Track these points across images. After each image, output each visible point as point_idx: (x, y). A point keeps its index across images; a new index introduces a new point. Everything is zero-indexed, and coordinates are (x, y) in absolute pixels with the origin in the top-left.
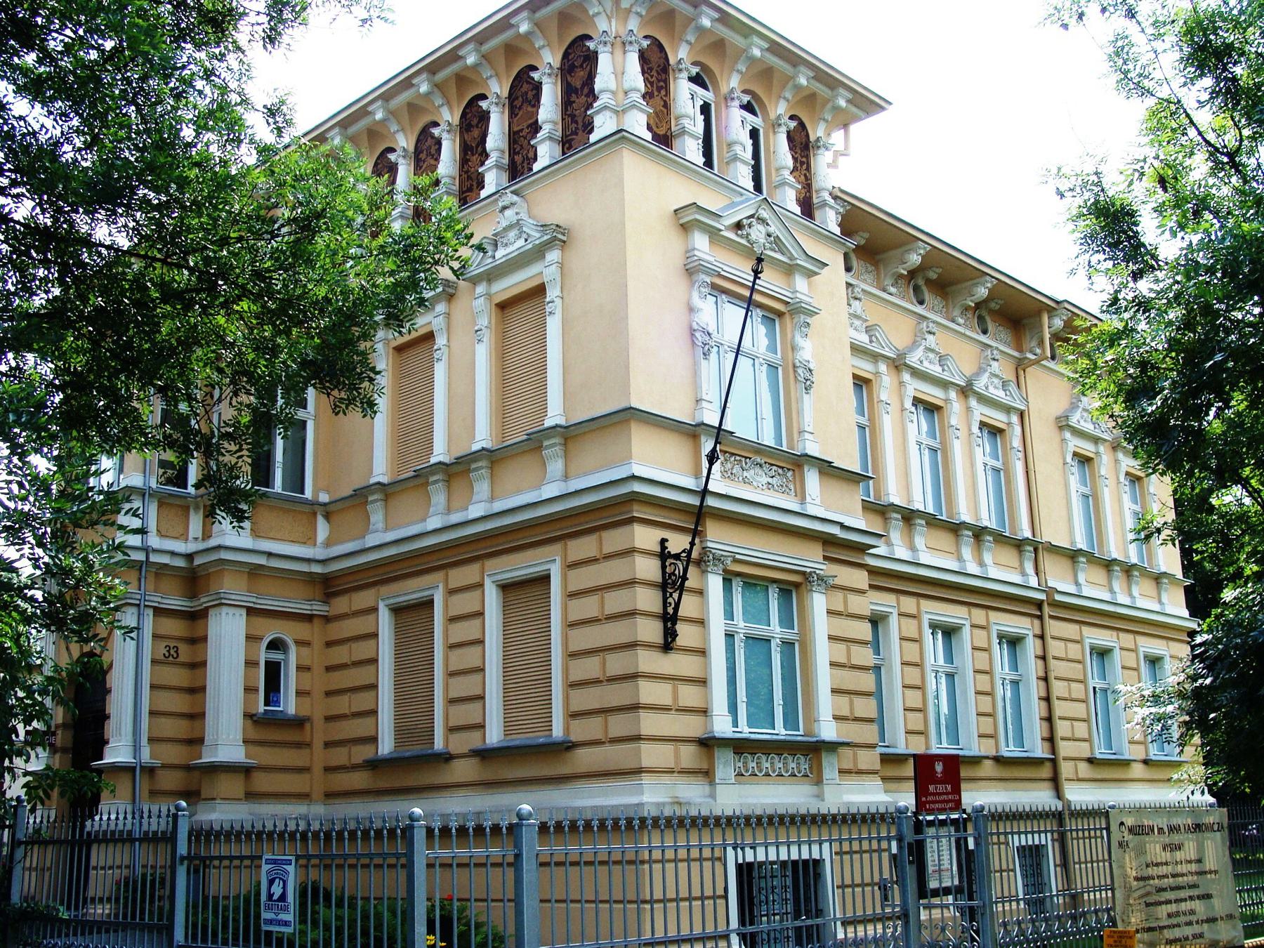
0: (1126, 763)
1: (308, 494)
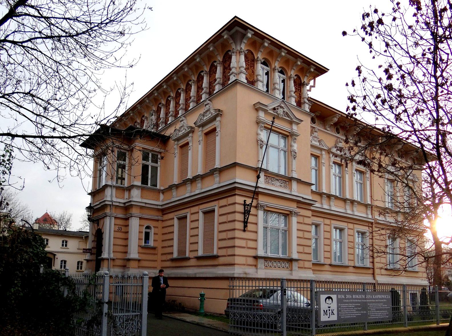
0: (323, 265)
1: (158, 187)
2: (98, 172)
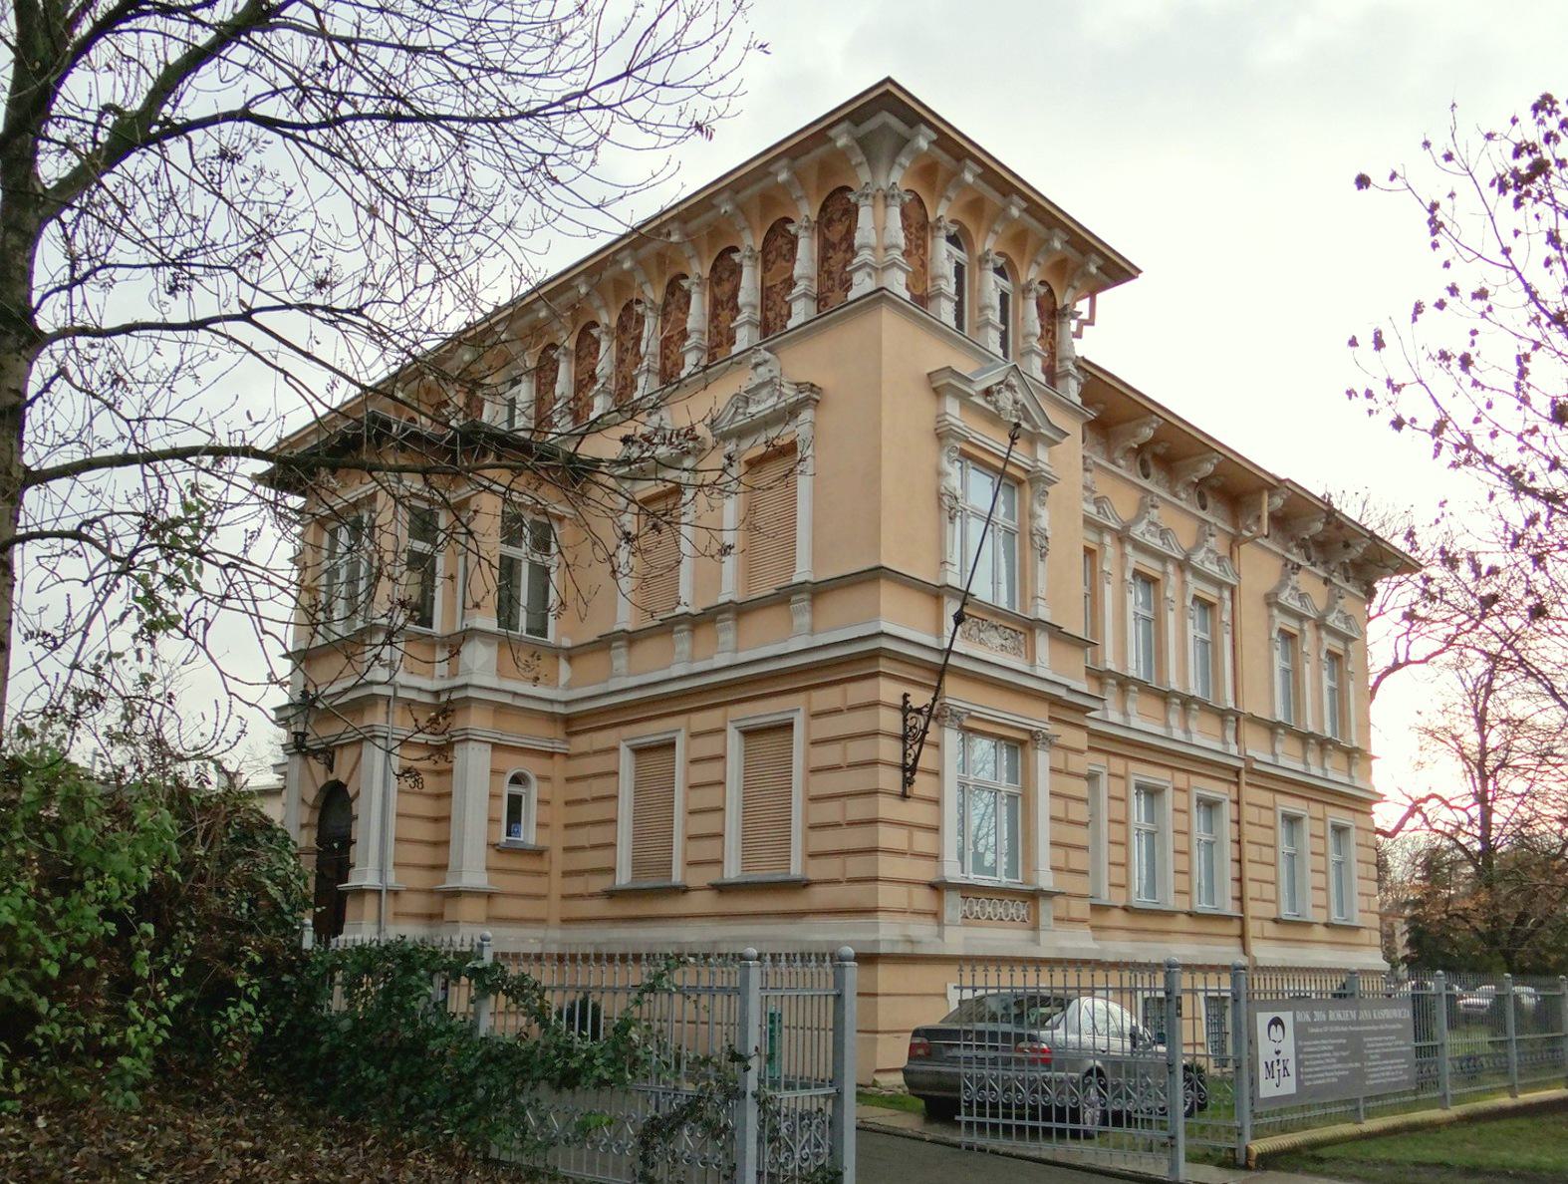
0: (1309, 925)
1: (551, 638)
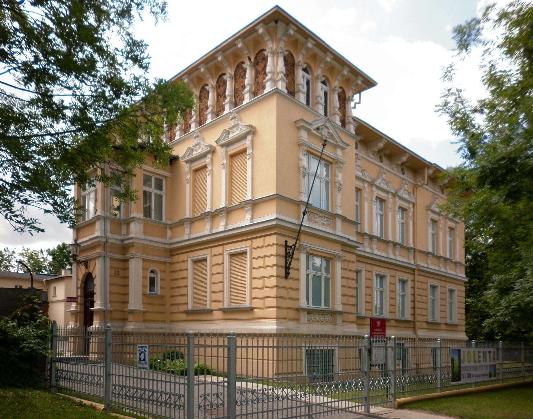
1: (164, 220)
2: (82, 198)
